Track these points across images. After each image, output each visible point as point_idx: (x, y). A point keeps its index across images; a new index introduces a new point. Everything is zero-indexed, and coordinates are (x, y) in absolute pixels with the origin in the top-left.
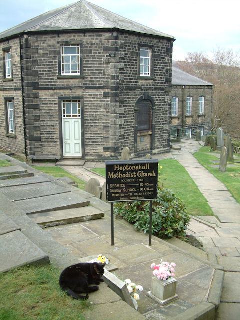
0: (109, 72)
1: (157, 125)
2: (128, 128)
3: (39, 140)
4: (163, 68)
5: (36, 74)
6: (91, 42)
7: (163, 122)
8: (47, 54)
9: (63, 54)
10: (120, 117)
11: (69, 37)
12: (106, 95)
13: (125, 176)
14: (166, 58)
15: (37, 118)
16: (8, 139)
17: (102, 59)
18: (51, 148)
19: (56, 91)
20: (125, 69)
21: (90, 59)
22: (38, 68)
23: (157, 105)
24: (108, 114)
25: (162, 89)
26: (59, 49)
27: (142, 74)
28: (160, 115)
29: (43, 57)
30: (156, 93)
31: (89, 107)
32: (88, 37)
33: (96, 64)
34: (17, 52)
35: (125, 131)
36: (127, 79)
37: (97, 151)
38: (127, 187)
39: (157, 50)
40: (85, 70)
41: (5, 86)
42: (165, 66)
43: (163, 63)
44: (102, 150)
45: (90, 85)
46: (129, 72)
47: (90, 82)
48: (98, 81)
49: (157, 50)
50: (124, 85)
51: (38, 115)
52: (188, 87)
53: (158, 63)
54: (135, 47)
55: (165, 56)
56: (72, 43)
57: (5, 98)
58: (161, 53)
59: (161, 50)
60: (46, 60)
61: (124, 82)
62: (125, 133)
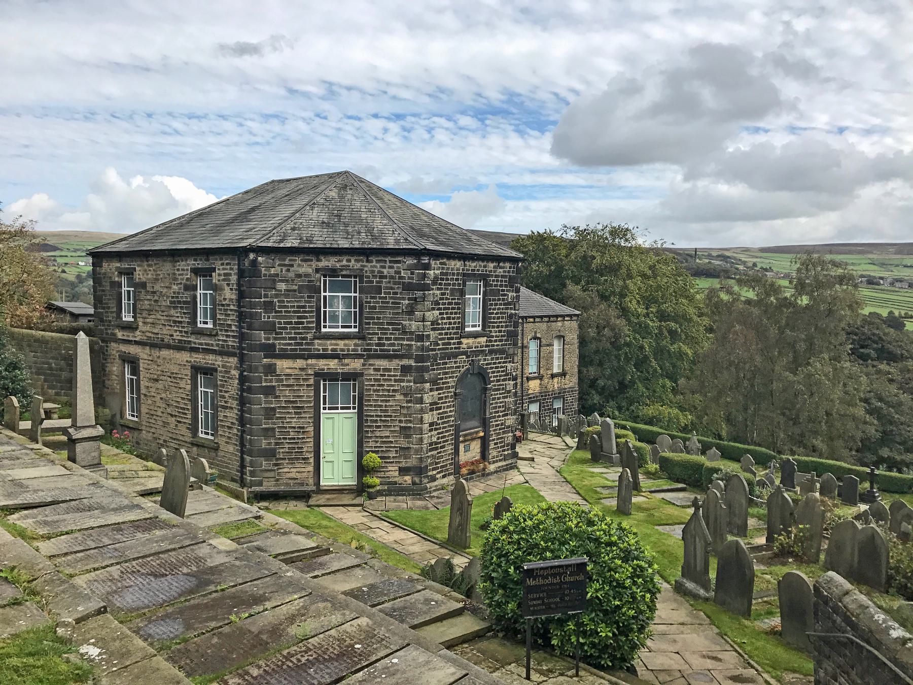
0: (414, 328)
1: (494, 417)
2: (444, 428)
3: (270, 454)
4: (504, 313)
5: (270, 328)
6: (379, 272)
7: (504, 411)
8: (295, 291)
9: (325, 291)
10: (432, 410)
11: (339, 261)
12: (405, 370)
13: (547, 581)
14: (510, 294)
15: (270, 413)
16: (195, 449)
17: (399, 303)
18: (298, 470)
19: (310, 361)
20: (440, 322)
21: (378, 302)
22: (276, 317)
23: (493, 381)
24: (409, 405)
25: (502, 352)
26: (318, 284)
27: (469, 326)
28: (499, 398)
29: (287, 296)
30: (492, 359)
31: (374, 391)
32: (374, 263)
33: (389, 314)
34: (230, 280)
35: (439, 434)
36: (443, 339)
37: (387, 474)
38: (549, 597)
39: (493, 281)
40: (369, 324)
41: (195, 343)
42: (507, 309)
43: (505, 304)
44: (397, 472)
45: (376, 350)
46: (448, 326)
47: (377, 345)
48: (393, 345)
49: (493, 281)
50: (439, 349)
51: (272, 406)
52: (532, 320)
53: (496, 304)
54: (457, 280)
55: (508, 291)
56: (344, 273)
57: (192, 367)
58: (502, 285)
59: (502, 281)
60: (291, 303)
61: (438, 345)
62: (438, 438)
